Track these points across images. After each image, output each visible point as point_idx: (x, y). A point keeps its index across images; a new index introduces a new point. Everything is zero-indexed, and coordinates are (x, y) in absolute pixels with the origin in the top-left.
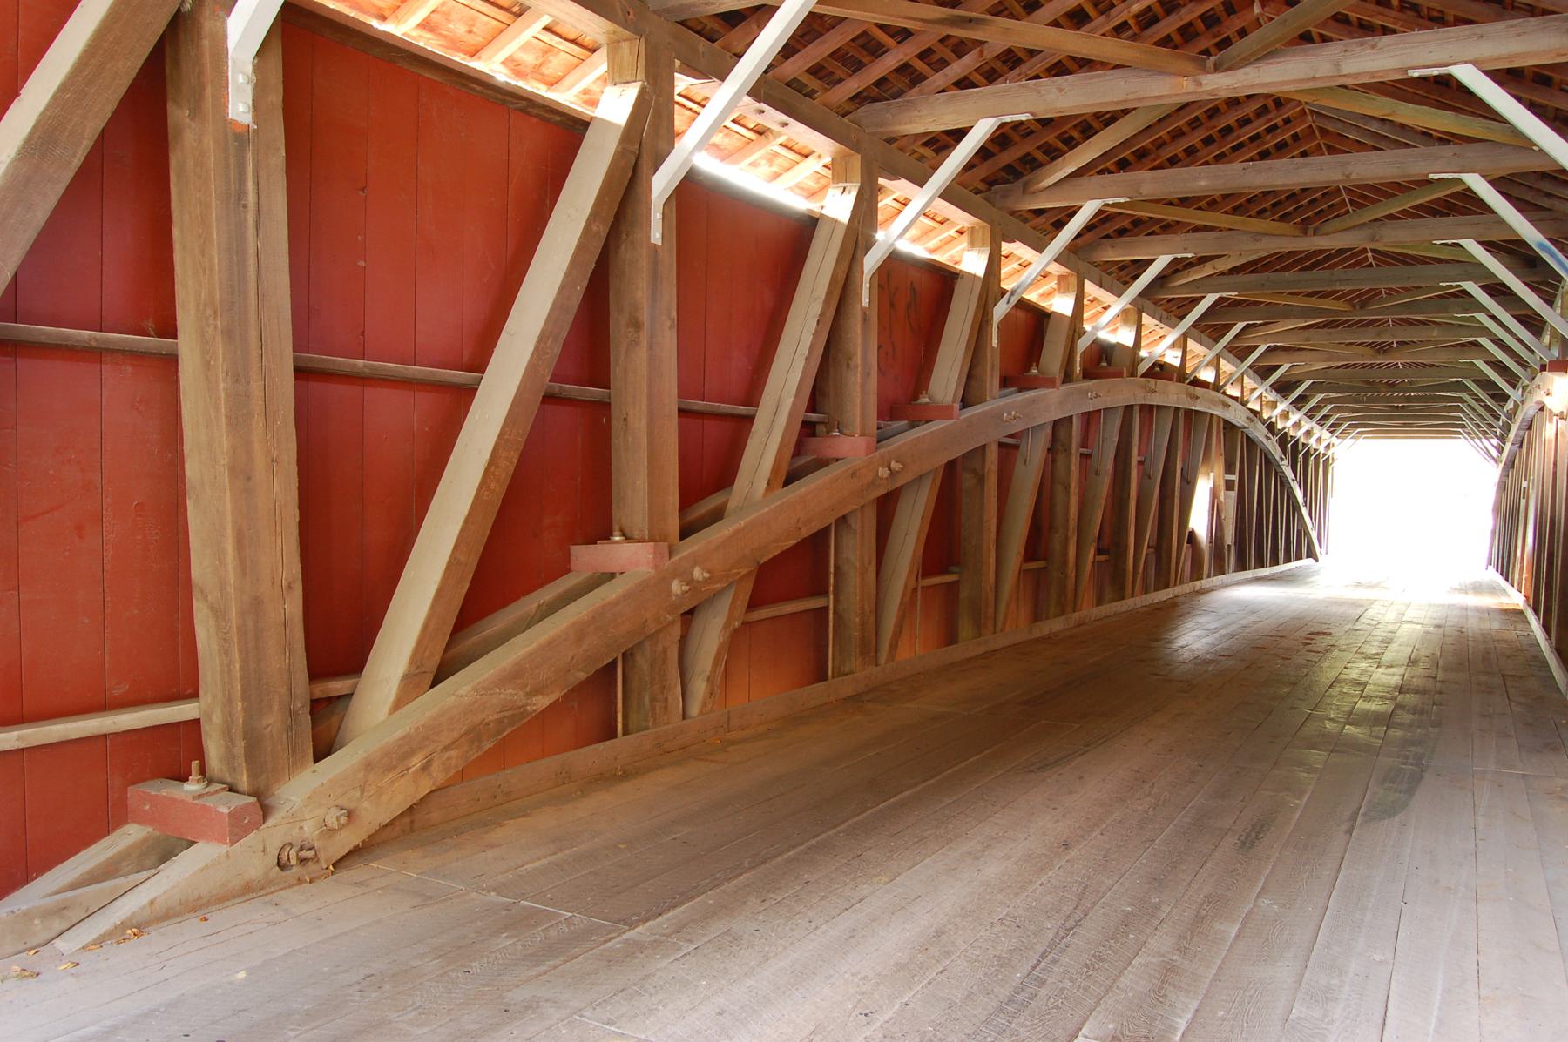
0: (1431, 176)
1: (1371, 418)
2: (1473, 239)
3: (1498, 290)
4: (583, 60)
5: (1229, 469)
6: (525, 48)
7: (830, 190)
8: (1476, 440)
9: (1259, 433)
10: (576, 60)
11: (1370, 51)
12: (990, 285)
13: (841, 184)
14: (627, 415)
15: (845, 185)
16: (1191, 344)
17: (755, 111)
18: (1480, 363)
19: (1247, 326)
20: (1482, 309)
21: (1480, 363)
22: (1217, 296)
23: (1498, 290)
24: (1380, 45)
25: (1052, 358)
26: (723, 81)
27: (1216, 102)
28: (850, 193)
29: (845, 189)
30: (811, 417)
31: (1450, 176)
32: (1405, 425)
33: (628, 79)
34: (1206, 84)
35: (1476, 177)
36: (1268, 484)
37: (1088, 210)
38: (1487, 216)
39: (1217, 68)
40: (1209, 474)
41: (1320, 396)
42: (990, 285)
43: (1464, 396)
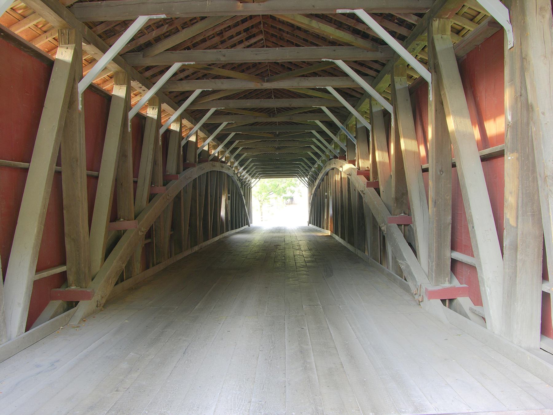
0: (323, 60)
1: (267, 171)
2: (331, 86)
3: (322, 133)
4: (40, 35)
5: (229, 193)
6: (26, 31)
7: (58, 48)
8: (303, 178)
9: (236, 178)
10: (18, 21)
11: (306, 81)
12: (158, 123)
13: (152, 106)
14: (122, 182)
15: (153, 107)
16: (185, 122)
17: (142, 90)
18: (309, 153)
19: (229, 123)
20: (315, 137)
21: (309, 153)
22: (227, 123)
23: (322, 133)
24: (309, 79)
25: (191, 158)
26: (149, 90)
27: (247, 16)
28: (155, 109)
29: (153, 108)
30: (21, 165)
31: (330, 60)
32: (277, 173)
33: (122, 83)
34: (264, 85)
35: (325, 107)
36: (237, 196)
37: (176, 67)
38: (324, 114)
39: (268, 81)
40: (224, 194)
41: (253, 164)
42: (158, 123)
43: (302, 163)
